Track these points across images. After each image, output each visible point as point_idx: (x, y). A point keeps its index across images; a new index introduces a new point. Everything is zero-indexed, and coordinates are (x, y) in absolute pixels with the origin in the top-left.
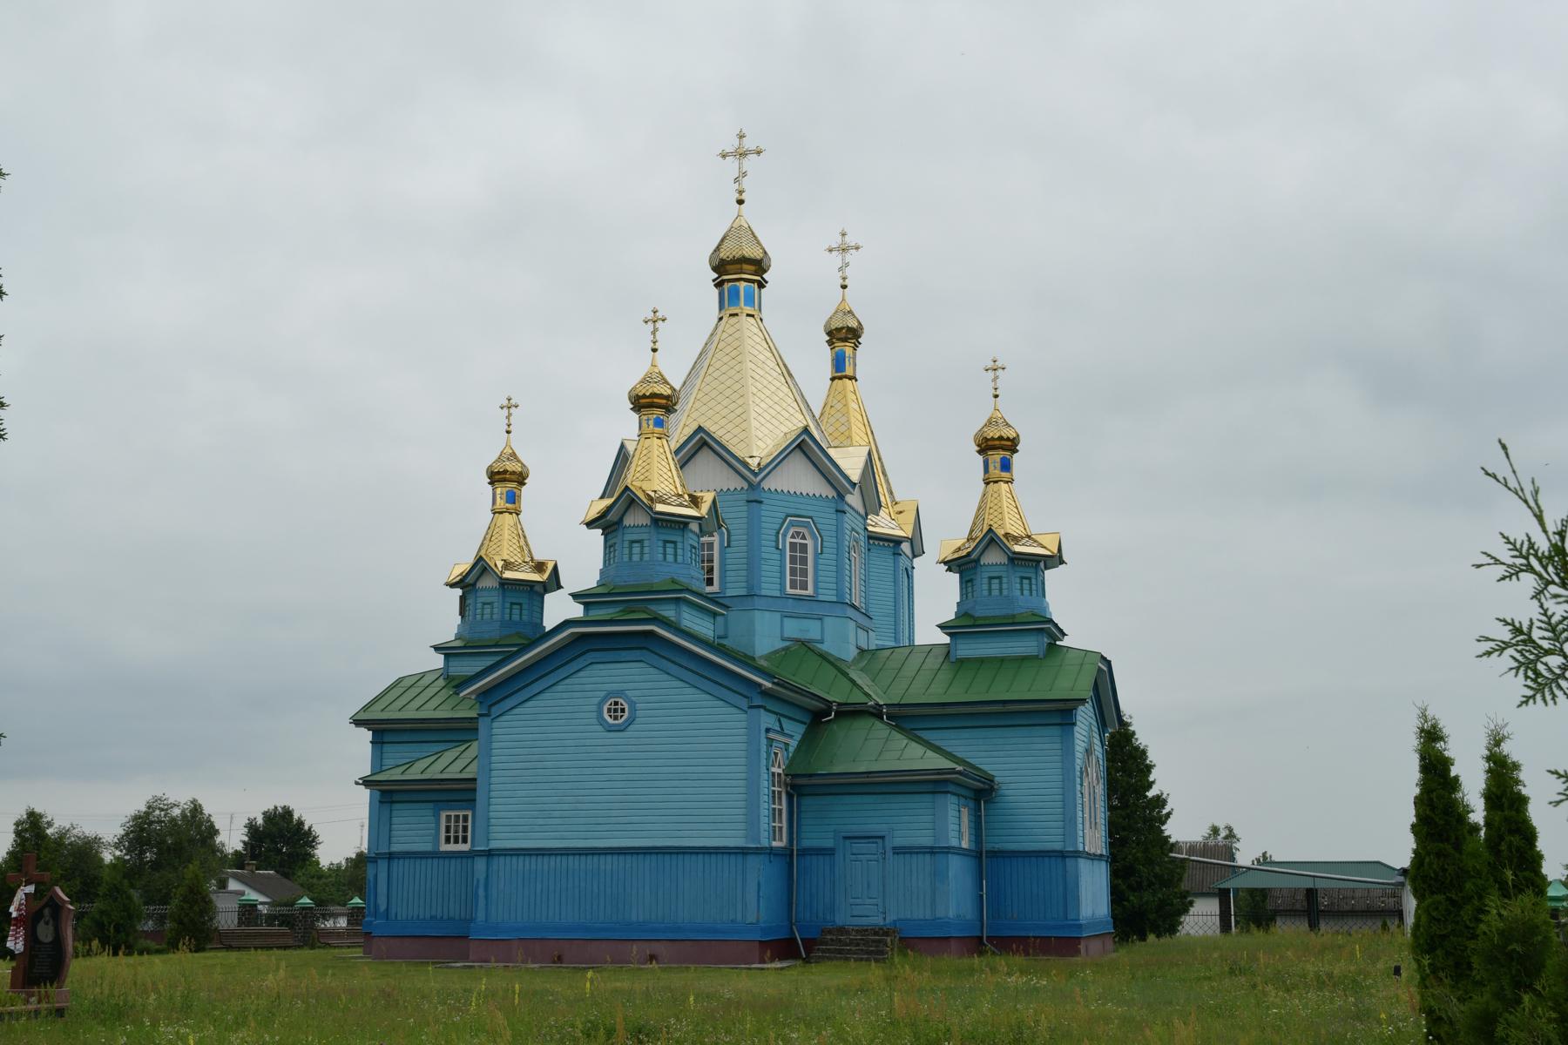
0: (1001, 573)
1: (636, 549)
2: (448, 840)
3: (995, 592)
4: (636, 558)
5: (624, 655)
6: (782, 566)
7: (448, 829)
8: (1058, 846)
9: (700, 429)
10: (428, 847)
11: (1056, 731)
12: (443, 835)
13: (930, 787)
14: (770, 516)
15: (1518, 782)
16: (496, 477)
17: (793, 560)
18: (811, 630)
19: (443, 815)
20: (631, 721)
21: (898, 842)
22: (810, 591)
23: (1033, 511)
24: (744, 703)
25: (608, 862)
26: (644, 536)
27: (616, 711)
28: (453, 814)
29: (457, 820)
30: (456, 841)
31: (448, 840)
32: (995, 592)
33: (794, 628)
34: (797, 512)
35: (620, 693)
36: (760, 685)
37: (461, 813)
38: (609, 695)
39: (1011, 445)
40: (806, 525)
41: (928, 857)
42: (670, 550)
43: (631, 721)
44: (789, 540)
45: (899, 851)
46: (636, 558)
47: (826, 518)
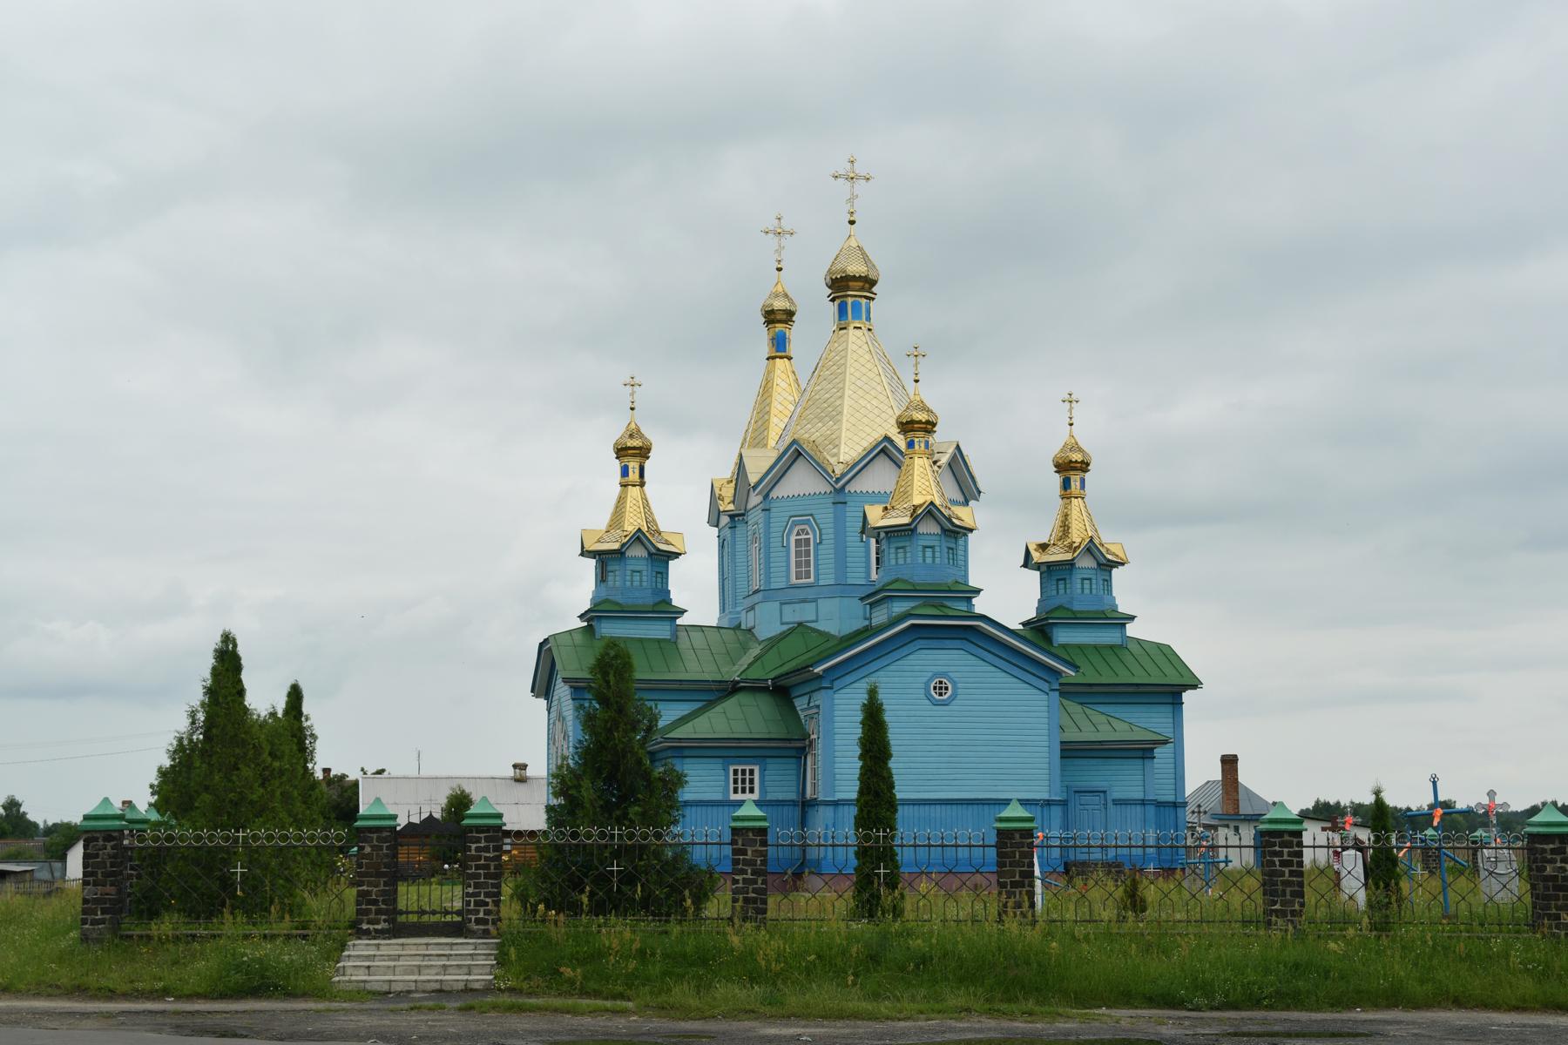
0: (1074, 577)
1: (929, 553)
2: (736, 791)
3: (1087, 591)
4: (929, 560)
5: (948, 643)
6: (788, 561)
7: (735, 781)
8: (1171, 798)
9: (794, 442)
10: (718, 797)
11: (1169, 708)
12: (732, 786)
13: (1140, 754)
14: (779, 516)
15: (273, 714)
16: (621, 452)
17: (798, 554)
18: (805, 613)
19: (731, 769)
20: (953, 697)
21: (1117, 795)
22: (812, 580)
23: (1099, 516)
24: (1045, 687)
25: (937, 811)
26: (936, 543)
27: (941, 689)
28: (740, 768)
29: (744, 772)
30: (744, 791)
31: (736, 791)
32: (1087, 591)
33: (794, 614)
34: (802, 516)
35: (944, 674)
36: (1057, 673)
37: (747, 768)
38: (935, 675)
39: (643, 452)
40: (803, 522)
41: (1139, 808)
42: (901, 555)
43: (953, 697)
44: (793, 538)
45: (1117, 802)
46: (929, 560)
47: (826, 515)
